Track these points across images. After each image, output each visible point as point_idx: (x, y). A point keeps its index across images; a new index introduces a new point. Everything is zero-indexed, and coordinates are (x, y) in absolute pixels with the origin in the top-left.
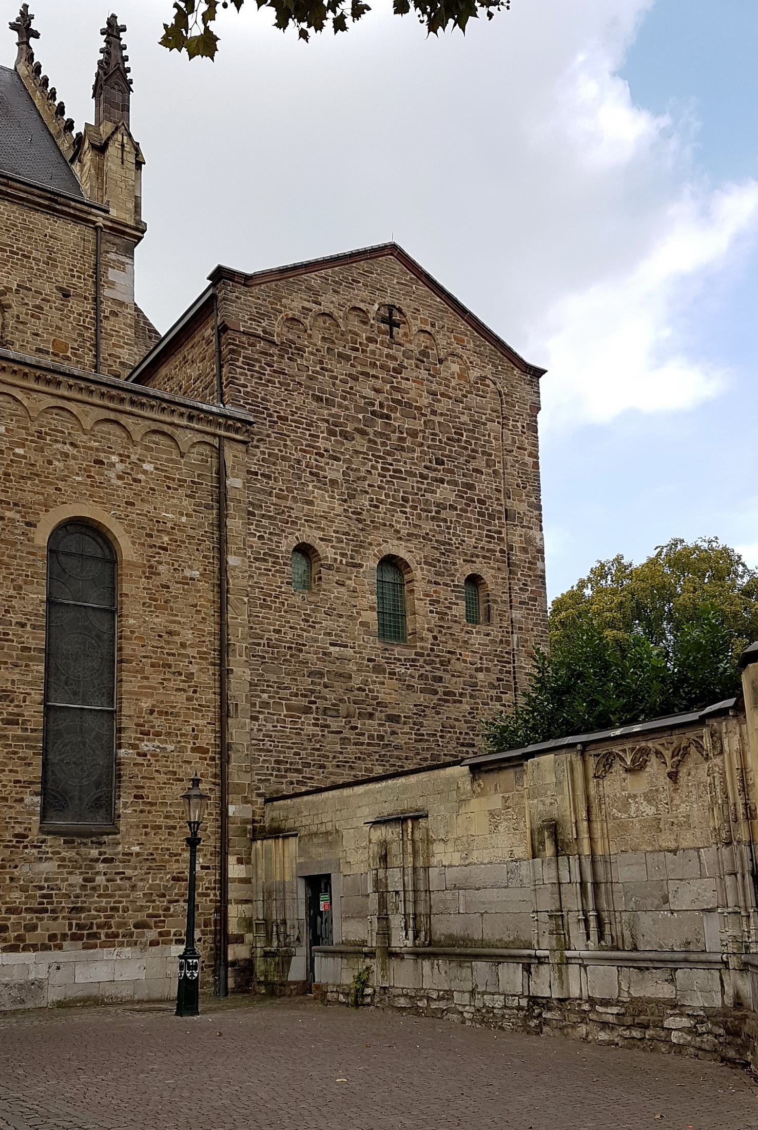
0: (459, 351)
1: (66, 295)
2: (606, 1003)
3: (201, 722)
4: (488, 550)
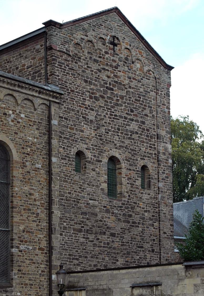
3: (42, 236)
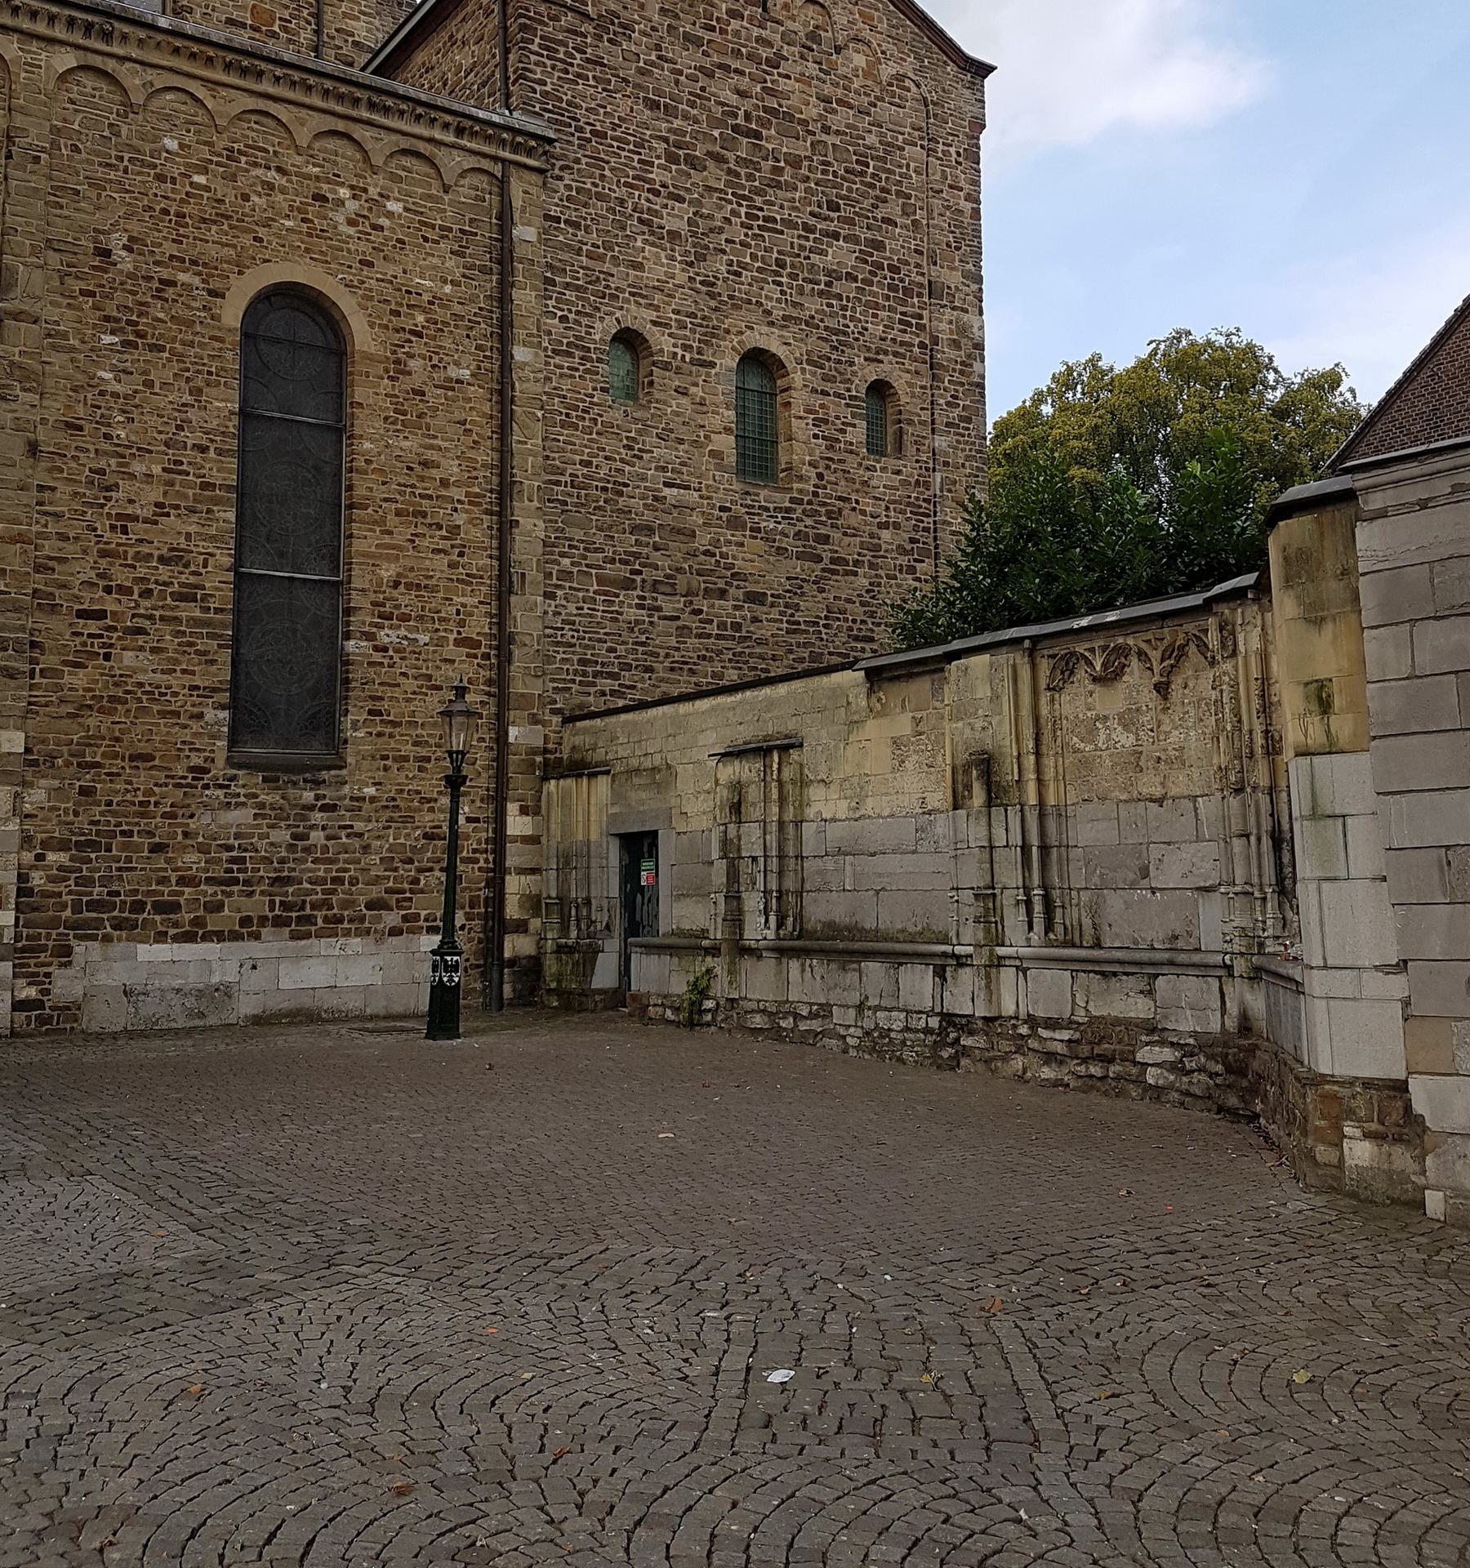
2: (1053, 1024)
4: (902, 344)
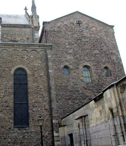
0: (95, 26)
1: (28, 39)
3: (45, 104)
4: (108, 61)
